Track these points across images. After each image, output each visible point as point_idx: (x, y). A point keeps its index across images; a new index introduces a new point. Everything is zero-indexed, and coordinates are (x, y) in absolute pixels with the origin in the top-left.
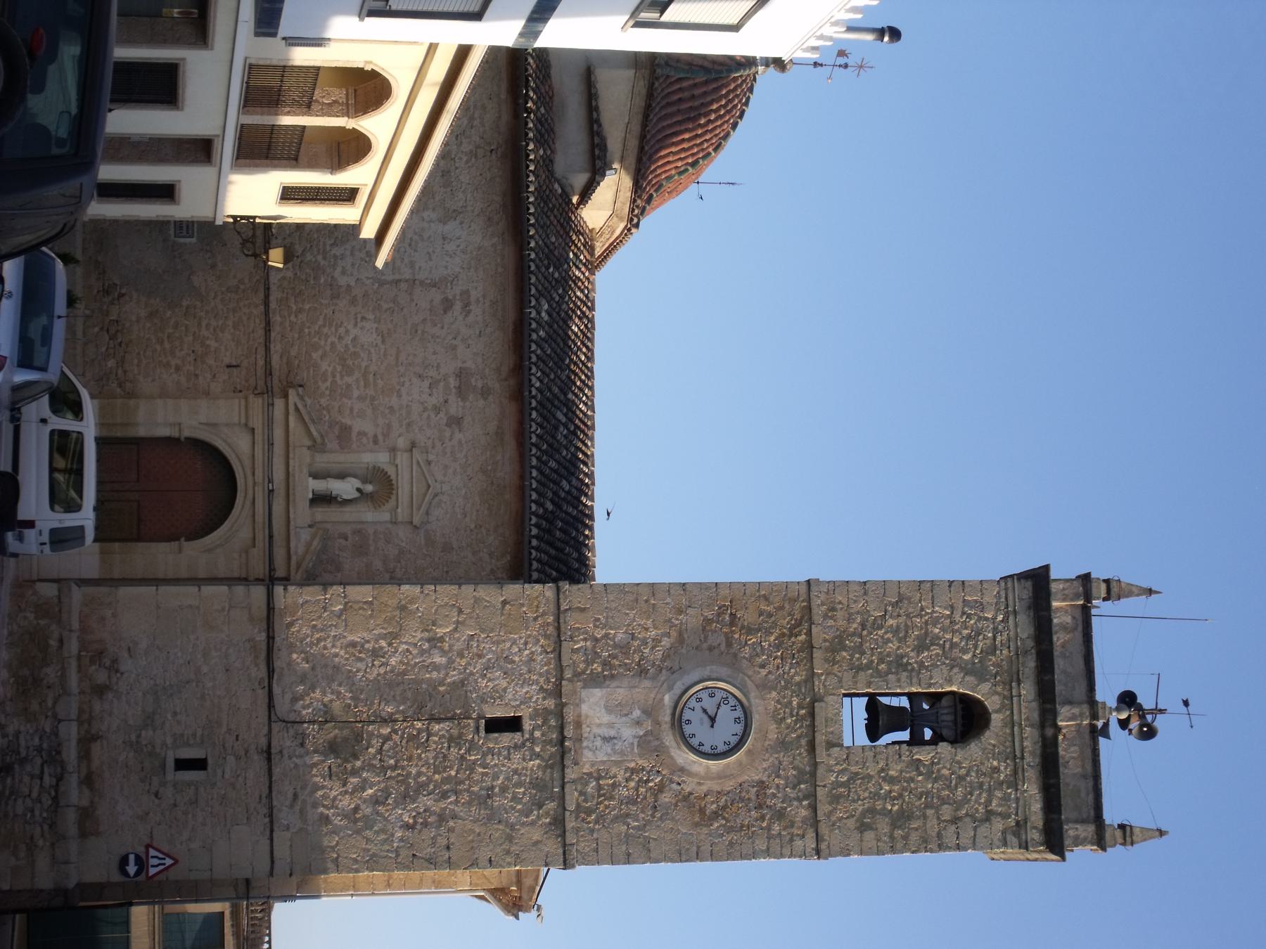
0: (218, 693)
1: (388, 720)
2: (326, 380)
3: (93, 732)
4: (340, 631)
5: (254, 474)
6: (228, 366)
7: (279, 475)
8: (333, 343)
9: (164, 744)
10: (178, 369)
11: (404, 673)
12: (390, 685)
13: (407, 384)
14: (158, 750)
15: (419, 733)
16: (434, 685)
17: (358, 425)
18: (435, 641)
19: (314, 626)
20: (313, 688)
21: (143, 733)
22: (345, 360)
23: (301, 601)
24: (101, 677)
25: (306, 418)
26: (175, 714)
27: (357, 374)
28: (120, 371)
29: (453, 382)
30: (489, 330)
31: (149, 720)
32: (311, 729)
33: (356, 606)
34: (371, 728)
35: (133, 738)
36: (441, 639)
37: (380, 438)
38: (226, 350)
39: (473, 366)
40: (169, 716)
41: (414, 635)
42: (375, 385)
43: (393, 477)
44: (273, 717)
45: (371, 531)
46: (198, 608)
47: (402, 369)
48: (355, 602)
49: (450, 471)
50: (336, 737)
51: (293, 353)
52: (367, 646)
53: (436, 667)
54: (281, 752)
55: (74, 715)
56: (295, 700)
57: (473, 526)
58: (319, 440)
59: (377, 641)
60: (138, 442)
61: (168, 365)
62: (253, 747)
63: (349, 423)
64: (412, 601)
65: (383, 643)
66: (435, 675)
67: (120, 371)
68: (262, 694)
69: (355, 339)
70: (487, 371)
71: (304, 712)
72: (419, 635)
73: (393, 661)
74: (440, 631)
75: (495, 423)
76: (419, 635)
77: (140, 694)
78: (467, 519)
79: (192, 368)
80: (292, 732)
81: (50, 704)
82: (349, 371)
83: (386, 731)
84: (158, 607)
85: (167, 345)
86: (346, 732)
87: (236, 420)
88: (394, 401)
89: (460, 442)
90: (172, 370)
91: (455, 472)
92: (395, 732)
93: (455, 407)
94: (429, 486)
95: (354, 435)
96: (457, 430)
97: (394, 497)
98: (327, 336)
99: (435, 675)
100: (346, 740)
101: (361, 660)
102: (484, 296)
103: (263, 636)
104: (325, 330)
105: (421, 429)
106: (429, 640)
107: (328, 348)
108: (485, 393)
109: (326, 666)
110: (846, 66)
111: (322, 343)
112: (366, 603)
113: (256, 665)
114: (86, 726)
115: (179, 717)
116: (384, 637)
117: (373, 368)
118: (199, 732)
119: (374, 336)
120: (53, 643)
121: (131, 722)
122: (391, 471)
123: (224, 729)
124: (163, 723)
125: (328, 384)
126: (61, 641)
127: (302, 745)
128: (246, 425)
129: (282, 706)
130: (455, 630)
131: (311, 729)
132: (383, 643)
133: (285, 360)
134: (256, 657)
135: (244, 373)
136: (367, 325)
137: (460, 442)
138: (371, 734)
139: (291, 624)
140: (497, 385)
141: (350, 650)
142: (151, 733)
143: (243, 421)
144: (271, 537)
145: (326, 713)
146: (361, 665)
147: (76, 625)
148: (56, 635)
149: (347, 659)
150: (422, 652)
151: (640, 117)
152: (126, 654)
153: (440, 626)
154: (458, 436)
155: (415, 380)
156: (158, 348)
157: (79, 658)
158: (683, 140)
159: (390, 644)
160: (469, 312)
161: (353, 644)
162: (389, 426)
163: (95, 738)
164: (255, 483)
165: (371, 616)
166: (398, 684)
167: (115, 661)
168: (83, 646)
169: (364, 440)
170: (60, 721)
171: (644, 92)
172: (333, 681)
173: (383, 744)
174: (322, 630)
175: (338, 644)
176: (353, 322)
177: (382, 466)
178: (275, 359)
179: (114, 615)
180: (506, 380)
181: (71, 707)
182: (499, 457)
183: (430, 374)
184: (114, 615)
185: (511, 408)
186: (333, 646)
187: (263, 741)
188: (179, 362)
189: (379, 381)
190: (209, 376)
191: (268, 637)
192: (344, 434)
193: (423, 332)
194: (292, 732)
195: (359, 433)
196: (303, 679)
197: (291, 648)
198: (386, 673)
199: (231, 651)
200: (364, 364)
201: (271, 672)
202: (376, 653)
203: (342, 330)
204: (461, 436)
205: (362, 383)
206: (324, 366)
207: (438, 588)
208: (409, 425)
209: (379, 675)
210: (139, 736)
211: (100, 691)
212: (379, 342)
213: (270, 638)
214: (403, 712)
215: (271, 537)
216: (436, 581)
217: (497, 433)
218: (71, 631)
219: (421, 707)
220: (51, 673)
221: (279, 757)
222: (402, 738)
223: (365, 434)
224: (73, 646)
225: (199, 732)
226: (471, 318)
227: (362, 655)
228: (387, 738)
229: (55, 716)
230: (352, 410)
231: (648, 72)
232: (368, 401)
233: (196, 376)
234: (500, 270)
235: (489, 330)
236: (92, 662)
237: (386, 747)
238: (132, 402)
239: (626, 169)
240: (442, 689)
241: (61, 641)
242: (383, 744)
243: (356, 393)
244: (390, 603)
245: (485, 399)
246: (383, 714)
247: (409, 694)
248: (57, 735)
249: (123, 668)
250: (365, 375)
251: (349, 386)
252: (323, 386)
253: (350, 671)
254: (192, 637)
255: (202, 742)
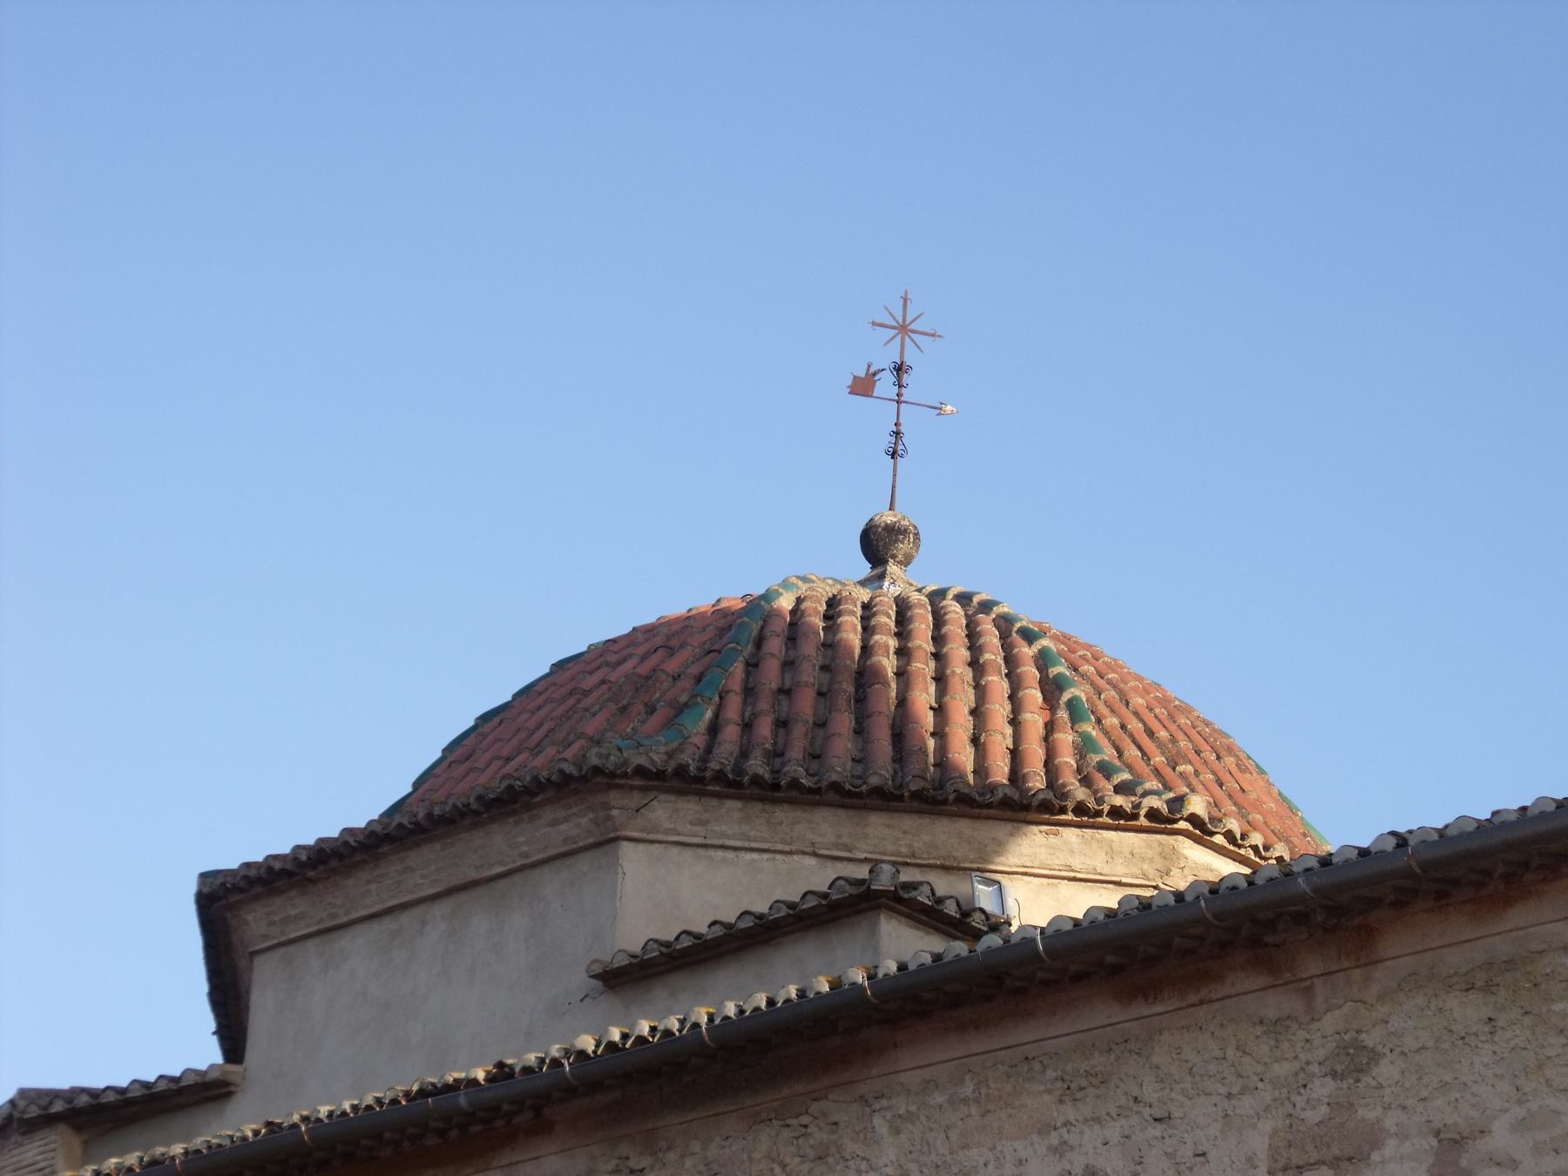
30: (1150, 1092)
70: (1283, 1069)
75: (1453, 1002)
89: (1521, 1126)
96: (1483, 1146)
102: (1046, 1128)
108: (1354, 1061)
110: (900, 369)
137: (1521, 1126)
140: (1330, 1022)
151: (782, 814)
158: (940, 710)
171: (690, 807)
180: (1308, 992)
185: (1403, 947)
204: (1500, 1126)
217: (1489, 988)
231: (614, 797)
234: (968, 1089)
239: (1000, 847)
245: (1374, 1057)
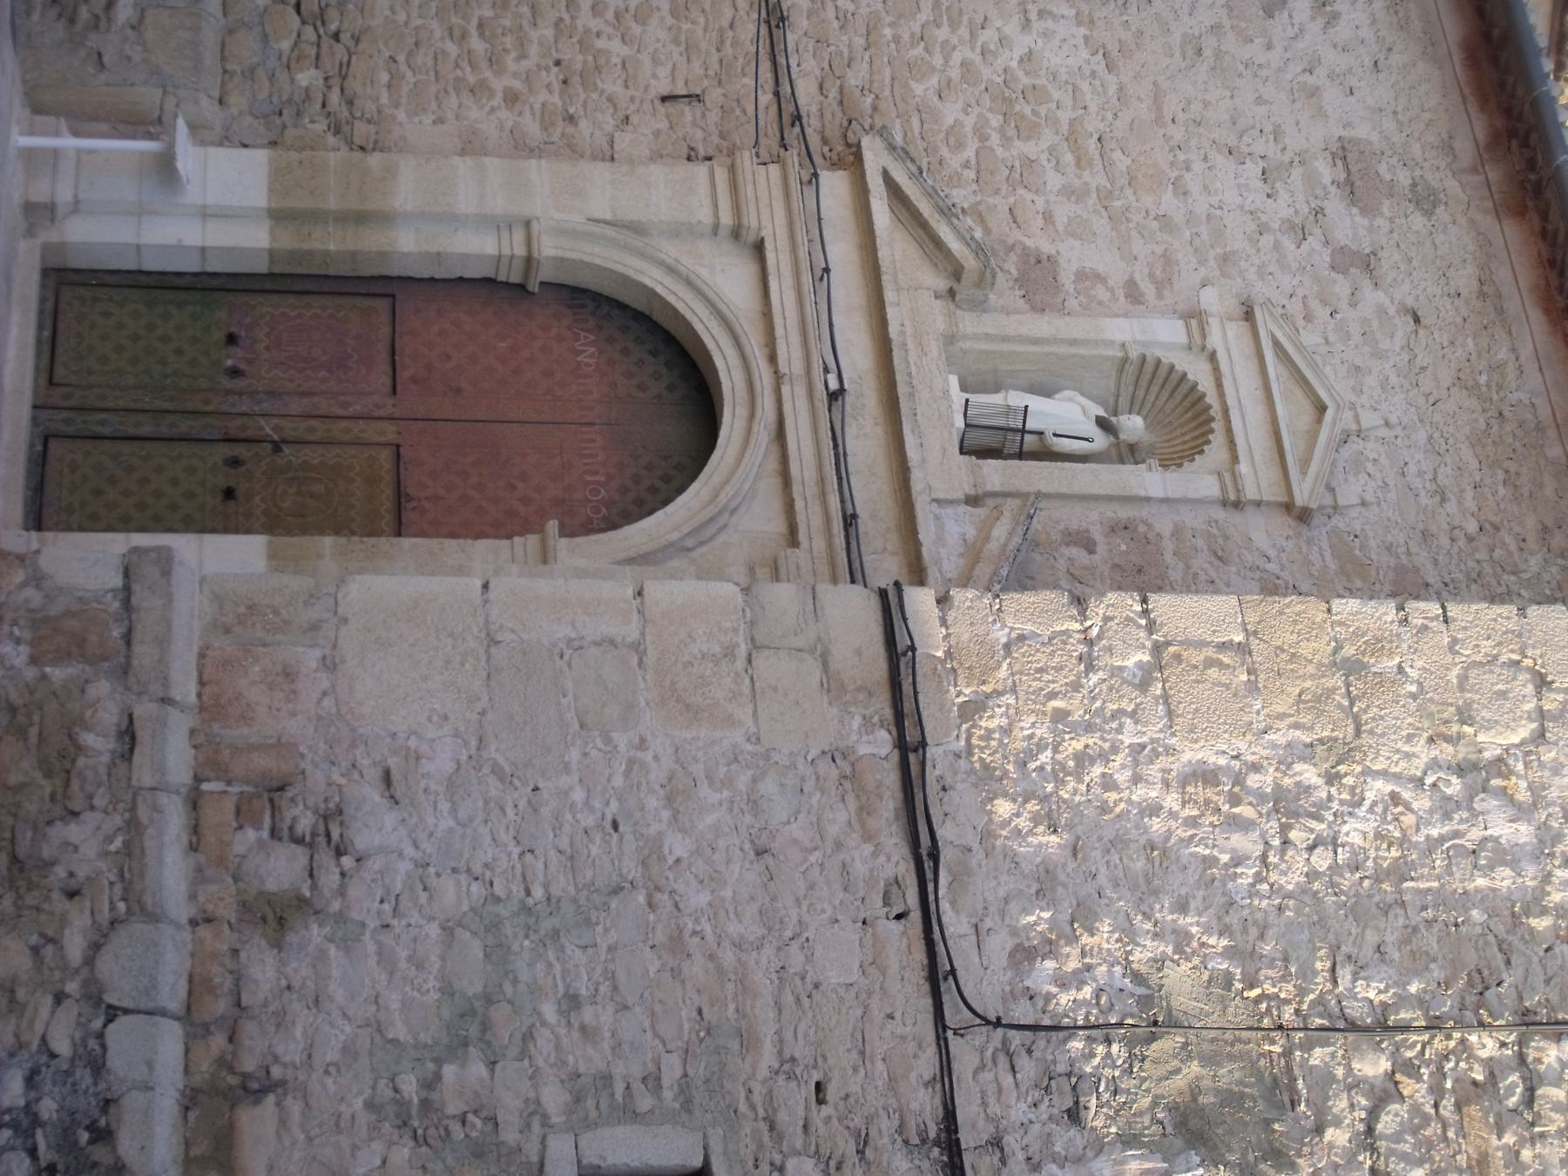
0: (733, 928)
1: (1381, 1027)
2: (960, 146)
3: (249, 1064)
4: (1153, 732)
5: (773, 358)
6: (664, 99)
7: (857, 358)
8: (966, 65)
9: (534, 1111)
10: (512, 98)
11: (1399, 872)
12: (1369, 911)
13: (1198, 167)
14: (510, 1136)
15: (1492, 1077)
16: (1513, 914)
17: (1072, 256)
18: (1481, 774)
19: (1060, 716)
20: (1084, 916)
21: (449, 1071)
22: (1009, 102)
23: (1002, 636)
24: (281, 869)
25: (925, 207)
26: (572, 1002)
27: (1048, 138)
28: (334, 98)
29: (1326, 171)
30: (1397, 59)
31: (470, 1026)
32: (1100, 1059)
33: (1197, 657)
34: (1318, 1056)
35: (410, 1085)
36: (1499, 766)
37: (1148, 289)
38: (655, 61)
39: (1375, 137)
40: (549, 1011)
41: (1402, 751)
42: (1108, 165)
43: (1206, 385)
44: (955, 1015)
45: (1164, 525)
46: (638, 648)
47: (1178, 133)
48: (1187, 643)
49: (1371, 381)
50: (1195, 1090)
51: (855, 78)
52: (1253, 780)
53: (1504, 856)
54: (996, 1143)
55: (172, 994)
56: (1025, 954)
57: (1472, 527)
58: (970, 262)
59: (1285, 765)
60: (387, 289)
61: (479, 90)
62: (886, 1125)
63: (1047, 248)
64: (1378, 646)
65: (1309, 774)
66: (1504, 879)
67: (334, 98)
68: (901, 943)
69: (1028, 57)
71: (1065, 999)
72: (1424, 753)
73: (1354, 832)
74: (1492, 742)
76: (1424, 753)
77: (434, 930)
78: (1451, 507)
79: (556, 99)
80: (1028, 1069)
81: (75, 946)
82: (1027, 130)
83: (1374, 1066)
84: (493, 642)
85: (477, 44)
86: (1229, 1074)
87: (704, 215)
88: (1169, 202)
89: (1381, 311)
90: (497, 101)
91: (1384, 384)
92: (1411, 1069)
93: (1346, 225)
94: (1321, 409)
95: (1066, 278)
96: (1366, 284)
97: (1218, 438)
98: (947, 49)
99: (1504, 879)
100: (1232, 1099)
101: (1236, 823)
103: (882, 743)
104: (943, 33)
105: (1262, 272)
106: (1460, 770)
107: (955, 73)
108: (1425, 199)
109: (1118, 843)
111: (938, 61)
112: (1222, 646)
113: (868, 837)
114: (218, 1041)
115: (588, 1014)
116: (1308, 752)
117: (1093, 125)
118: (672, 1070)
119: (1085, 54)
120: (99, 743)
121: (400, 1032)
122: (1198, 372)
123: (768, 1058)
124: (528, 1036)
125: (970, 153)
126: (128, 734)
127: (1074, 1115)
128: (736, 233)
129: (983, 977)
130: (1540, 736)
131: (1100, 1059)
132: (1309, 774)
133: (833, 93)
134: (864, 810)
135: (713, 117)
136: (1062, 29)
138: (1323, 1080)
139: (972, 710)
140: (1452, 185)
141: (1197, 791)
142: (478, 1070)
143: (726, 219)
144: (850, 520)
145: (1145, 1002)
146: (1246, 843)
147: (186, 689)
148: (109, 716)
149: (1192, 822)
150: (1447, 806)
152: (373, 794)
153: (1489, 726)
154: (1371, 297)
155: (1219, 159)
156: (452, 49)
157: (195, 801)
159: (1332, 778)
160: (1335, 16)
161: (1208, 776)
162: (1167, 260)
163: (257, 1088)
164: (778, 377)
165: (1253, 688)
166: (1385, 910)
167: (332, 815)
168: (210, 763)
169: (1101, 293)
170: (112, 1013)
172: (1156, 892)
173: (1373, 1114)
174: (1089, 728)
175: (1153, 771)
176: (1016, 19)
177: (1168, 357)
178: (806, 92)
179: (329, 665)
181: (160, 963)
182: (1503, 354)
183: (1259, 147)
184: (329, 665)
186: (1136, 779)
187: (924, 1105)
188: (517, 85)
189: (1117, 155)
190: (609, 121)
191: (902, 745)
192: (1039, 281)
193: (1218, 54)
194: (1028, 1069)
195: (1081, 275)
196: (1045, 884)
197: (989, 781)
198: (1335, 868)
199: (769, 786)
200: (1065, 116)
201: (925, 858)
202: (1287, 805)
203: (988, 36)
204: (1381, 297)
205: (1069, 158)
206: (951, 112)
207: (1454, 610)
208: (1225, 259)
209: (1312, 875)
210: (431, 1083)
211: (276, 916)
212: (1101, 67)
213: (910, 752)
214: (1421, 1002)
215: (850, 520)
216: (1447, 591)
218: (166, 701)
219: (1482, 984)
220: (84, 844)
221: (989, 1160)
222: (1437, 1091)
223: (1099, 278)
224: (173, 754)
225: (672, 1070)
226: (1342, 32)
227: (1245, 811)
228: (1384, 1094)
229: (94, 995)
230: (1048, 217)
232: (1092, 200)
233: (571, 119)
235: (1397, 59)
236: (243, 814)
237: (1387, 1123)
238: (374, 160)
240: (1541, 924)
241: (128, 734)
242: (1373, 1114)
243: (1054, 181)
244: (1305, 649)
245: (1428, 214)
246: (1355, 1010)
247: (1430, 941)
248: (98, 1066)
249: (362, 840)
250: (1073, 138)
251: (1029, 163)
252: (954, 162)
253: (1210, 862)
254: (621, 740)
255: (687, 1106)
